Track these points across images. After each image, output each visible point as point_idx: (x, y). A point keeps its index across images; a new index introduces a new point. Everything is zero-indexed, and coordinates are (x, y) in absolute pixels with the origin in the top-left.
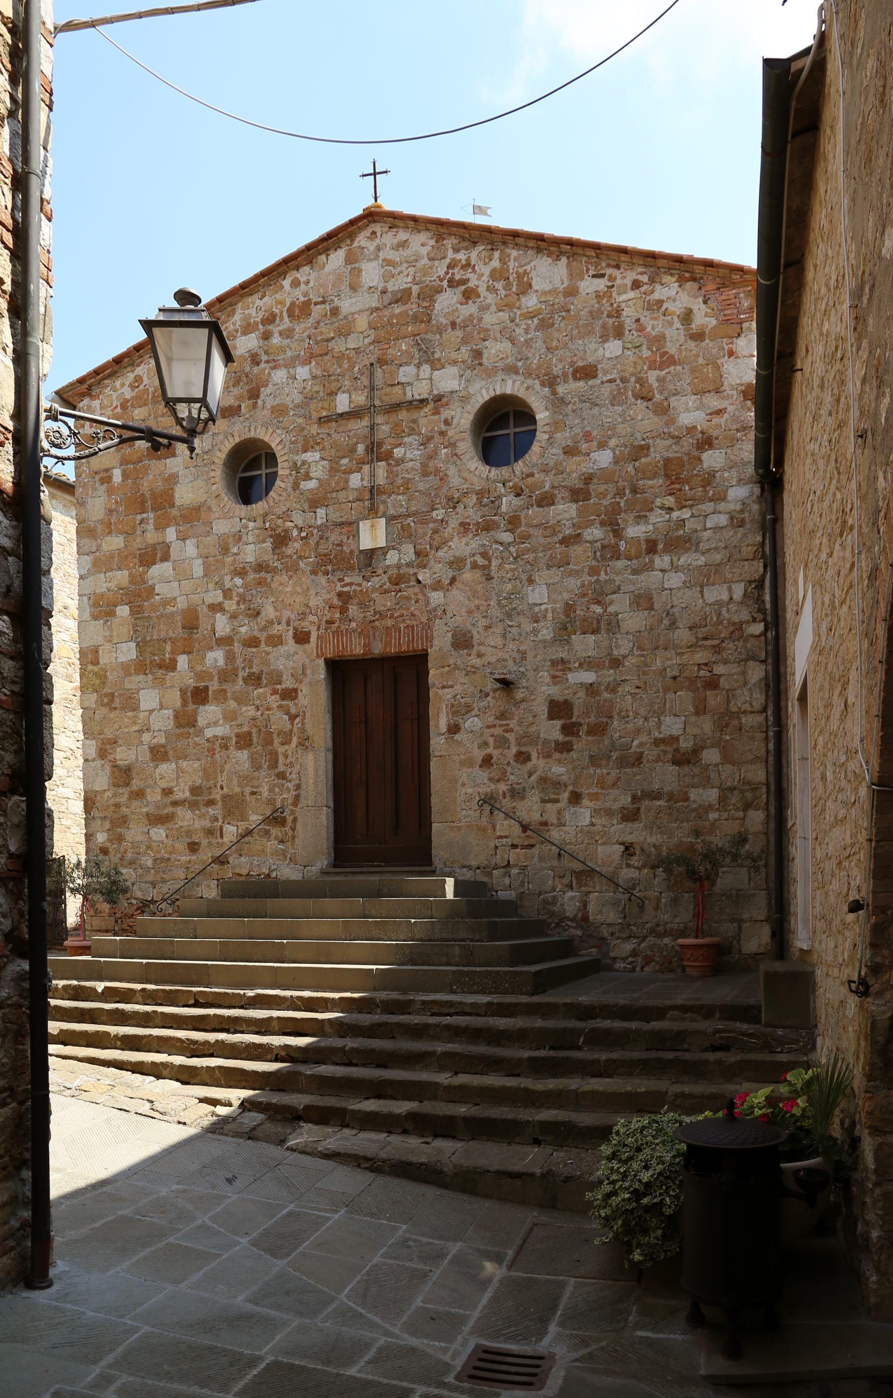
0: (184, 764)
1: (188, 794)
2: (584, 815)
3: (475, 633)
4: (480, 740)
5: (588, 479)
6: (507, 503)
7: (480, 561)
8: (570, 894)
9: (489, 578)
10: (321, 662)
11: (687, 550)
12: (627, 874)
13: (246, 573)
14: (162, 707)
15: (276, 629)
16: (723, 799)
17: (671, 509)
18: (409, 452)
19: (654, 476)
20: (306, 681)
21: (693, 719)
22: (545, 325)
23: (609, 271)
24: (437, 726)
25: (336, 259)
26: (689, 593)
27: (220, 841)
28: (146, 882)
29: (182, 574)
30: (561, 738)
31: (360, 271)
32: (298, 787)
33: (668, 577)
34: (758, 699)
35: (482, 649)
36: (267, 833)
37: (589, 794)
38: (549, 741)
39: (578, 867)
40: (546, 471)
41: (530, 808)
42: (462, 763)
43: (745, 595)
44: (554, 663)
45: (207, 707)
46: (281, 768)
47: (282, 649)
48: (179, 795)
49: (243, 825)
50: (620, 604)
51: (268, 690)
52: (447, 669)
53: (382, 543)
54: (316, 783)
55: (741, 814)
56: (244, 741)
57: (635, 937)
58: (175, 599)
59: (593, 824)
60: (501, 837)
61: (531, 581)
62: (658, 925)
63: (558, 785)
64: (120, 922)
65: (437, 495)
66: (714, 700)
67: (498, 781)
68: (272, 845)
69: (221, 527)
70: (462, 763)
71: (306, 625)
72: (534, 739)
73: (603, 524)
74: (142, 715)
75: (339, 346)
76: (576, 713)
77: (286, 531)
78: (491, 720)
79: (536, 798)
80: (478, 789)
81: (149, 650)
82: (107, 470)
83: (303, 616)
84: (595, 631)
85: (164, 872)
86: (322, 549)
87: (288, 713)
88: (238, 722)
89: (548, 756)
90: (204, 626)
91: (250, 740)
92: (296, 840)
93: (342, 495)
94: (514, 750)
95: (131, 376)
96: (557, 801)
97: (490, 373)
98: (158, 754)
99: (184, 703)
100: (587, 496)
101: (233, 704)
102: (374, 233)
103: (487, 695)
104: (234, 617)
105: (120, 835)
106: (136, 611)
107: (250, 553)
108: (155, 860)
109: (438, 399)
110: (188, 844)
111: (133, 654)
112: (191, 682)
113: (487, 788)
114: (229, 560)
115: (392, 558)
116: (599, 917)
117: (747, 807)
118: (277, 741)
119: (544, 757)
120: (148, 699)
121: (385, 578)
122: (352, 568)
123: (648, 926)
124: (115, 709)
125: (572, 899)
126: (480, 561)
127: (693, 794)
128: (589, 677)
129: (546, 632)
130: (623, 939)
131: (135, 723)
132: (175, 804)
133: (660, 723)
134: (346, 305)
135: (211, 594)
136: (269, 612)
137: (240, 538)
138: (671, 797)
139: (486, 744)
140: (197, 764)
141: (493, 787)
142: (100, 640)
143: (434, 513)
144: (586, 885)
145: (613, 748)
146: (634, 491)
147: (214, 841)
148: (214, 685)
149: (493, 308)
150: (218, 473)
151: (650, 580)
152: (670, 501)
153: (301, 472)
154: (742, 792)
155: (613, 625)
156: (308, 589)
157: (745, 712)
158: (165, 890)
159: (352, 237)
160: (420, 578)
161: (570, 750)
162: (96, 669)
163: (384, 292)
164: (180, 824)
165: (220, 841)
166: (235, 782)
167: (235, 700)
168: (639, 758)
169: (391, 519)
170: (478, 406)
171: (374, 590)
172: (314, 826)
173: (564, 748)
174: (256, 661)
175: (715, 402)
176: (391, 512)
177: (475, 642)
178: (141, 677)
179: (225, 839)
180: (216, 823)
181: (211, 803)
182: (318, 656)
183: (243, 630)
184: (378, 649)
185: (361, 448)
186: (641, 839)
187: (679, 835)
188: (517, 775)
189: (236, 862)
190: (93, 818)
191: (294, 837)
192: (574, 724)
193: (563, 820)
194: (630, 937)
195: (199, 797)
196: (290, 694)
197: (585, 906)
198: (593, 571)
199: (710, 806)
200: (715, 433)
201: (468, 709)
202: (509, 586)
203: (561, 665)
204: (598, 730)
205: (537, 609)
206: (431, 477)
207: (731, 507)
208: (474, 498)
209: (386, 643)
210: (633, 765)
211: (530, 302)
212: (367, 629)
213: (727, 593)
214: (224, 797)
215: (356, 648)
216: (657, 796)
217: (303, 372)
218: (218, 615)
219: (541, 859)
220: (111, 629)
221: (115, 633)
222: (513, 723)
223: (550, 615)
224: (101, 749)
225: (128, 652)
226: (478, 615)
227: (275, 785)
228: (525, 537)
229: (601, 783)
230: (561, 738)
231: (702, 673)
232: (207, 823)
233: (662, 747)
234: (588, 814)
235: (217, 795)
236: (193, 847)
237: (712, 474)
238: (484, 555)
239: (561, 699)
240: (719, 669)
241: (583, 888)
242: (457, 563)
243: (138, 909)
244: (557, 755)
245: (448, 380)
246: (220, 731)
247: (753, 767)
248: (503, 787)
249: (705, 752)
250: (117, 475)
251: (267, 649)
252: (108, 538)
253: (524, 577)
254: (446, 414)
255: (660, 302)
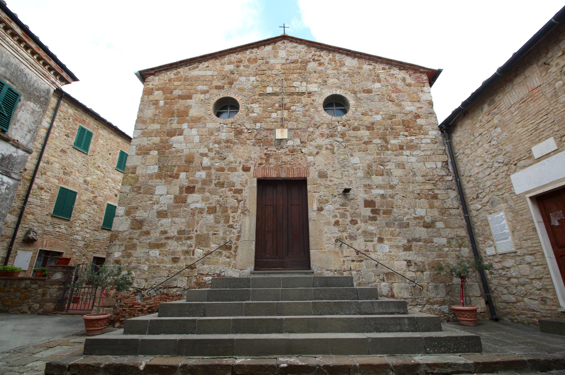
0: (176, 219)
1: (176, 234)
2: (386, 247)
3: (328, 172)
4: (334, 214)
5: (373, 124)
6: (340, 128)
7: (329, 147)
8: (383, 284)
9: (333, 153)
10: (255, 179)
11: (416, 150)
12: (409, 275)
13: (221, 143)
14: (168, 193)
15: (233, 165)
16: (449, 242)
17: (407, 136)
18: (298, 108)
19: (399, 125)
20: (247, 186)
21: (429, 210)
22: (351, 76)
23: (373, 64)
24: (312, 208)
25: (269, 48)
26: (419, 164)
27: (192, 256)
28: (142, 279)
29: (187, 141)
30: (371, 215)
31: (278, 52)
32: (240, 232)
33: (410, 158)
34: (456, 204)
35: (332, 179)
36: (220, 253)
37: (387, 239)
38: (366, 216)
39: (386, 270)
40: (355, 119)
41: (360, 244)
42: (325, 224)
43: (442, 166)
44: (365, 186)
45: (193, 195)
46: (231, 223)
47: (236, 173)
48: (171, 234)
49: (207, 249)
50: (390, 166)
51: (228, 189)
52: (316, 185)
53: (286, 137)
54: (250, 230)
55: (458, 249)
56: (211, 210)
57: (420, 305)
58: (183, 150)
59: (390, 252)
60: (346, 257)
61: (352, 155)
62: (430, 299)
63: (372, 234)
64: (119, 301)
65: (310, 124)
66: (437, 203)
67: (343, 231)
68: (223, 259)
69: (210, 125)
70: (325, 224)
71: (249, 165)
72: (359, 215)
73: (380, 138)
74: (155, 197)
75: (268, 72)
76: (377, 205)
77: (242, 130)
78: (338, 206)
79: (362, 240)
80: (333, 235)
81: (165, 169)
82: (157, 101)
83: (247, 161)
84: (382, 175)
85: (154, 273)
86: (258, 137)
87: (237, 199)
88: (209, 202)
89: (366, 222)
90: (197, 161)
91: (215, 210)
92: (237, 257)
93: (268, 120)
94: (349, 219)
95: (175, 71)
96: (372, 241)
97: (330, 88)
98: (161, 214)
99: (181, 192)
100: (373, 129)
101: (208, 194)
102: (284, 42)
103: (335, 196)
104: (213, 159)
105: (130, 253)
106: (161, 153)
107: (223, 136)
108: (149, 267)
109: (309, 93)
110: (173, 258)
111: (156, 170)
112: (186, 184)
113: (338, 235)
114: (213, 137)
115: (290, 143)
116: (399, 295)
117: (460, 246)
118: (229, 211)
119: (364, 222)
120: (161, 189)
121: (287, 150)
122: (272, 145)
123: (425, 299)
124: (141, 193)
125: (385, 286)
126: (329, 147)
127: (435, 240)
128: (382, 192)
129: (360, 174)
130: (413, 306)
131: (151, 200)
132: (168, 238)
133: (415, 211)
134: (272, 61)
135: (202, 149)
136: (231, 158)
137: (219, 130)
138: (425, 241)
139: (336, 216)
140: (183, 220)
141: (340, 234)
142: (138, 163)
143: (309, 129)
144: (391, 279)
145: (395, 220)
146: (392, 129)
147: (188, 257)
148: (198, 186)
149: (330, 69)
150: (211, 107)
151: (403, 158)
152: (406, 133)
153: (249, 111)
154: (457, 240)
155: (389, 173)
156: (251, 151)
157: (451, 208)
158: (153, 283)
159: (275, 42)
160: (303, 151)
161: (376, 220)
162: (133, 175)
163: (287, 59)
164: (169, 248)
165: (192, 256)
166: (205, 228)
167: (209, 192)
168: (408, 225)
169: (290, 130)
170: (326, 97)
171: (281, 154)
172: (247, 251)
173: (374, 219)
174: (222, 177)
175: (418, 105)
176: (290, 127)
177: (329, 176)
178: (159, 180)
179: (195, 256)
180: (191, 248)
181: (189, 238)
182: (254, 177)
183: (217, 164)
184: (283, 175)
185: (277, 105)
186: (414, 259)
187: (432, 257)
188: (352, 229)
189: (201, 268)
190: (115, 245)
191: (235, 255)
192: (377, 210)
193: (376, 249)
194: (417, 305)
195: (182, 235)
196: (239, 191)
197: (392, 289)
198: (378, 154)
199: (444, 245)
200: (420, 114)
201: (327, 201)
202: (342, 157)
203: (368, 187)
204: (388, 212)
205: (355, 165)
206: (307, 117)
207: (431, 137)
208: (326, 126)
209: (287, 174)
210: (406, 227)
211: (345, 69)
212: (278, 167)
213: (435, 165)
214: (197, 236)
215: (273, 174)
216: (419, 240)
217: (253, 79)
218: (205, 158)
219: (367, 267)
220: (145, 159)
221: (148, 161)
222: (348, 208)
223: (361, 168)
224: (127, 211)
225: (154, 169)
226: (329, 166)
227: (227, 231)
228: (348, 141)
229: (392, 234)
230: (371, 215)
231: (430, 193)
232: (185, 248)
233: (418, 220)
234: (387, 247)
235: (193, 235)
236: (175, 260)
237: (422, 126)
238: (331, 145)
239: (370, 199)
240: (437, 192)
241: (390, 281)
242: (319, 147)
243: (133, 293)
244: (370, 222)
245: (313, 88)
246: (199, 205)
247: (459, 230)
248: (345, 234)
249: (437, 223)
250: (162, 103)
251: (229, 173)
252: (152, 125)
253: (349, 154)
254: (313, 98)
255: (393, 75)
